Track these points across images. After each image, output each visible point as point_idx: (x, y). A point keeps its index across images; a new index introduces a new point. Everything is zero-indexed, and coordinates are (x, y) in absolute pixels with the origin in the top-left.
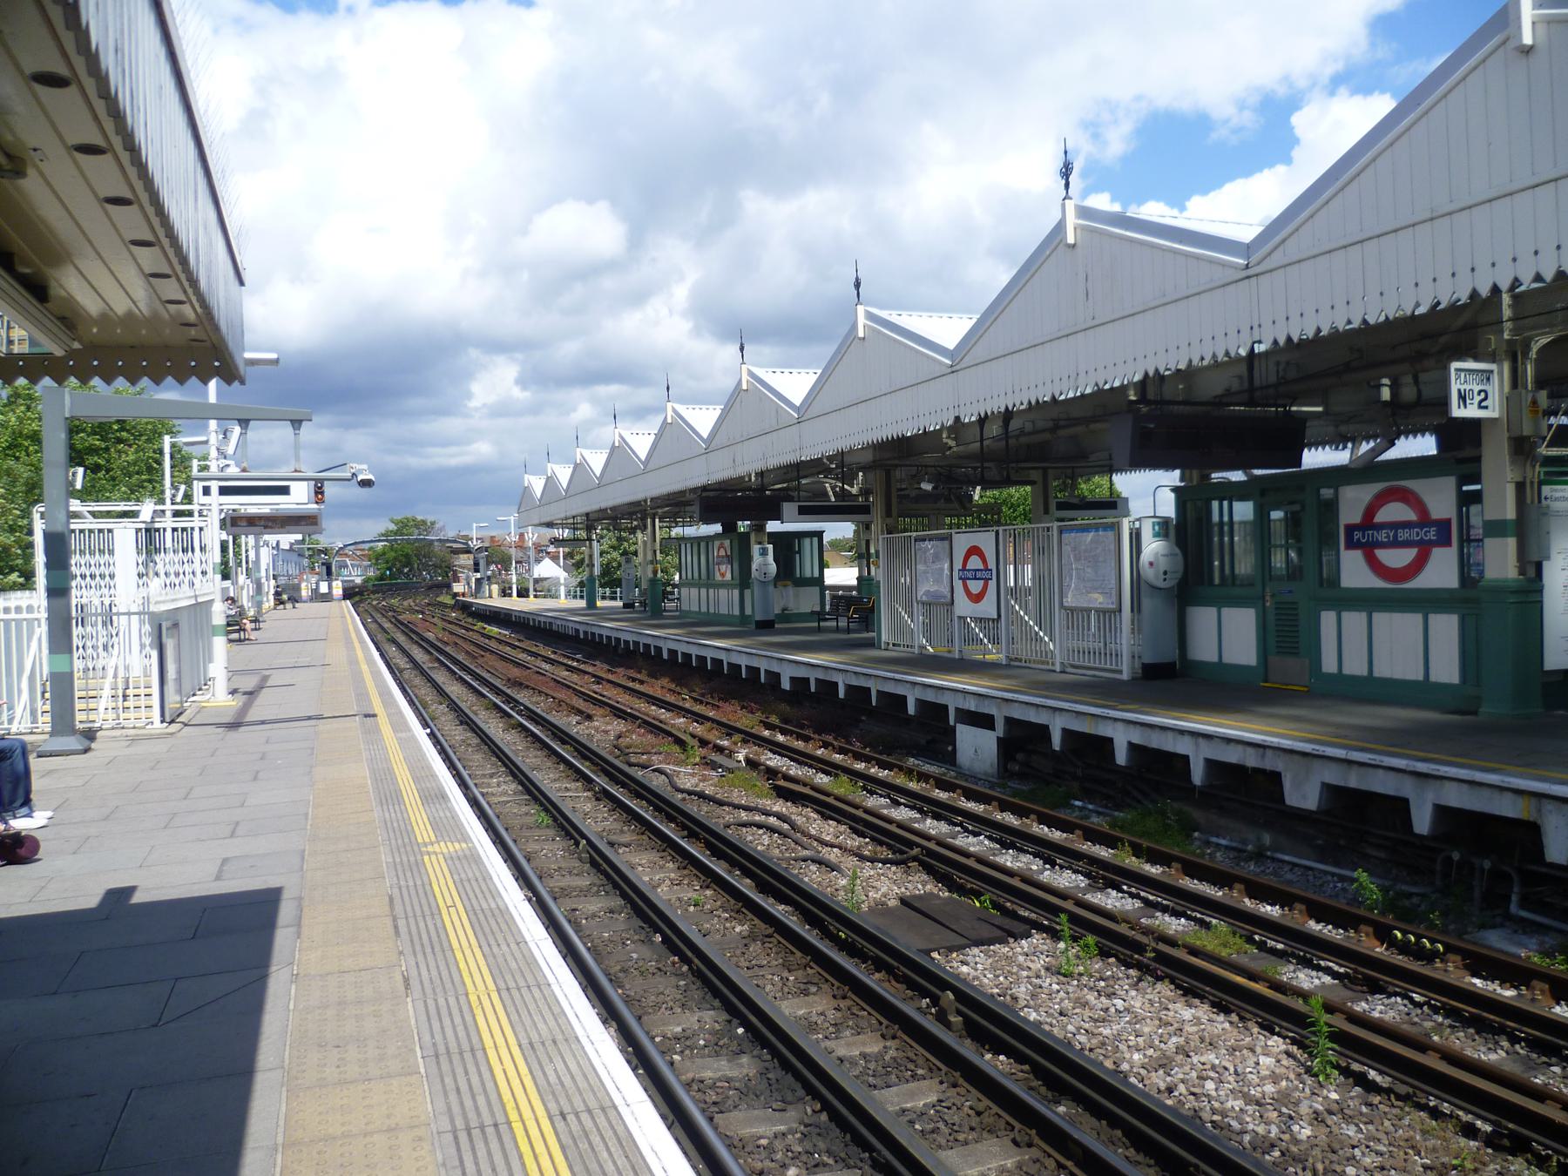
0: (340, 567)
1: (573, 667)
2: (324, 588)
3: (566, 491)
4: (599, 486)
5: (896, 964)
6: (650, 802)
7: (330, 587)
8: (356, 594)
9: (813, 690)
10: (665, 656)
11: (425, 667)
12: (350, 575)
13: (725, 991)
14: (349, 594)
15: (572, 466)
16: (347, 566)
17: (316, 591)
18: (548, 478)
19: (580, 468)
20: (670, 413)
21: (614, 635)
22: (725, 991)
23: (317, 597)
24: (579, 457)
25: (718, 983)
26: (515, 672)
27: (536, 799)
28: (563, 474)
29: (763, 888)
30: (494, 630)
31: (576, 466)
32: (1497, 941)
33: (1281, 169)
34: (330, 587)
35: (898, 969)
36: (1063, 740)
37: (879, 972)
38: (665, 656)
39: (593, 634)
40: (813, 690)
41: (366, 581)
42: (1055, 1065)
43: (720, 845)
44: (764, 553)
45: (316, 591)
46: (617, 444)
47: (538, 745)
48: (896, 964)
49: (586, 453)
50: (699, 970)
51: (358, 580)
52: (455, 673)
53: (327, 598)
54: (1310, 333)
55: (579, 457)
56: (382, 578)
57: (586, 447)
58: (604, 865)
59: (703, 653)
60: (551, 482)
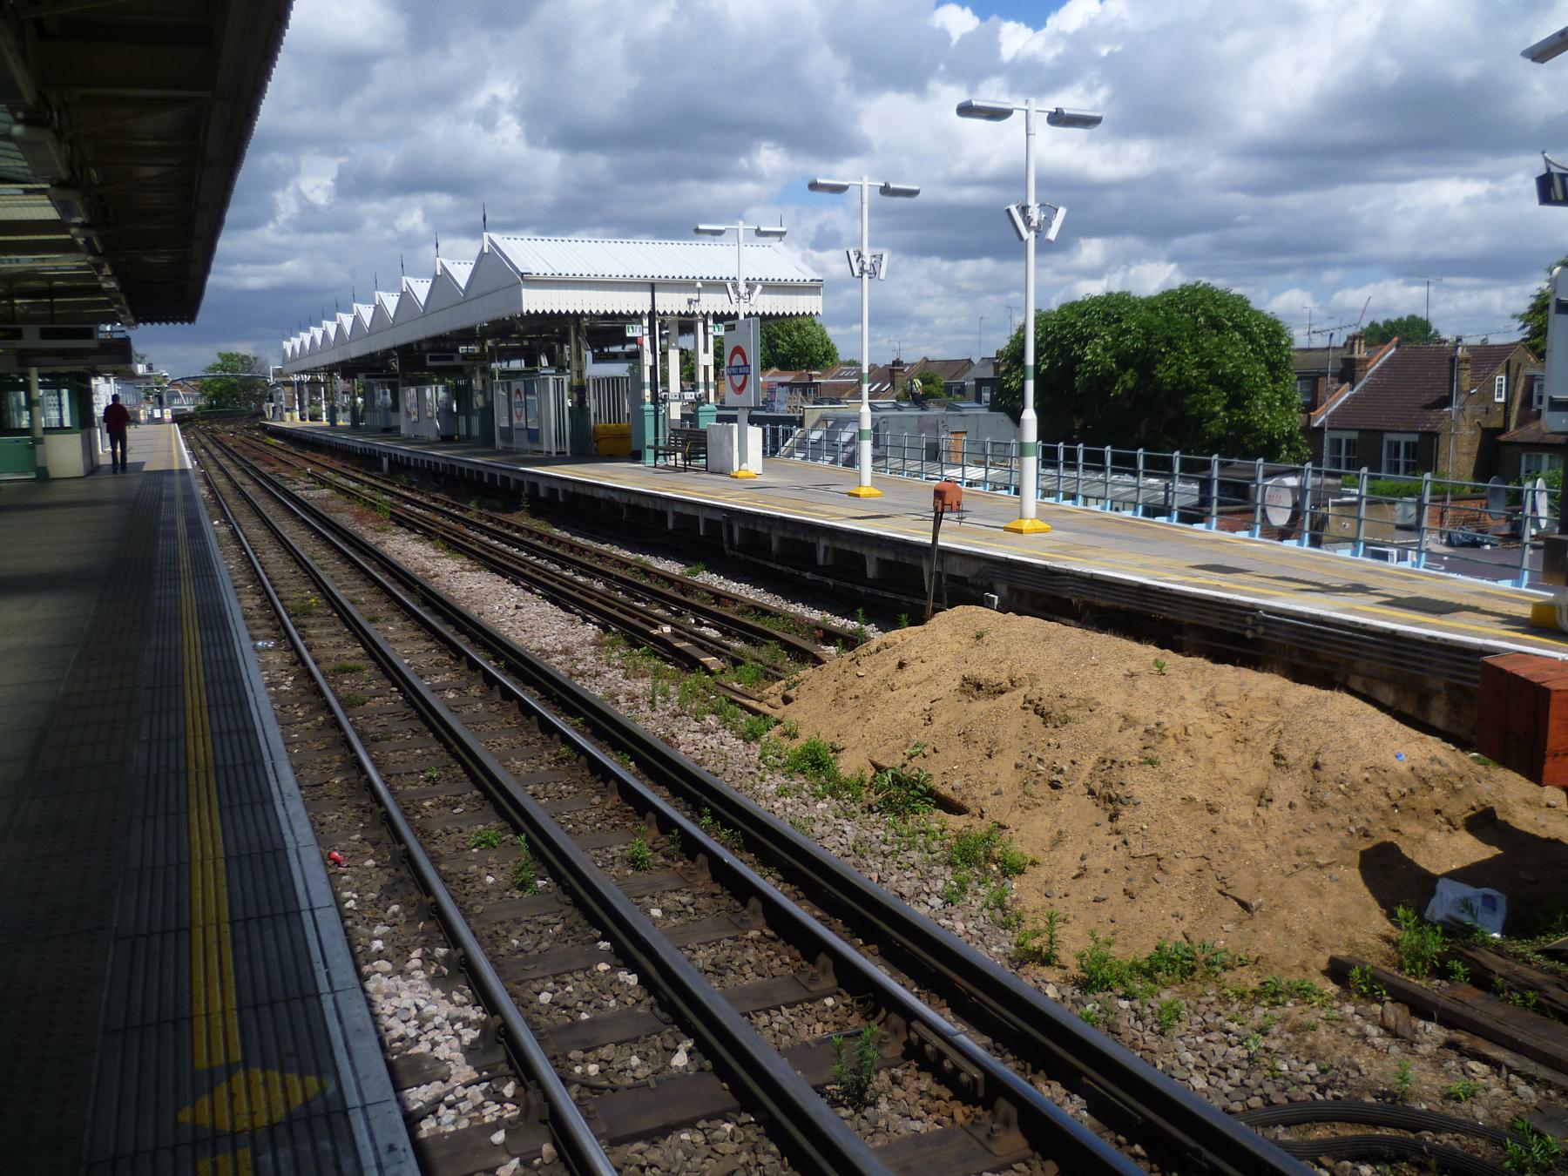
0: (173, 397)
1: (516, 539)
2: (157, 414)
3: (425, 308)
4: (369, 335)
5: (1192, 1144)
6: (635, 757)
7: (162, 413)
8: (186, 420)
9: (670, 526)
10: (486, 480)
11: (423, 686)
12: (182, 404)
13: (721, 1049)
14: (179, 418)
15: (431, 281)
16: (179, 396)
17: (151, 416)
18: (402, 293)
19: (406, 298)
20: (486, 243)
21: (413, 457)
22: (721, 1049)
23: (152, 420)
24: (404, 285)
25: (491, 787)
26: (255, 453)
27: (319, 589)
28: (391, 302)
29: (511, 670)
30: (273, 441)
31: (436, 278)
32: (438, 495)
33: (1030, 31)
34: (162, 413)
35: (1198, 1153)
36: (675, 523)
37: (749, 851)
38: (486, 480)
39: (422, 461)
40: (670, 526)
41: (199, 408)
42: (1042, 1033)
43: (671, 774)
44: (385, 393)
45: (151, 416)
46: (486, 250)
47: (385, 596)
48: (1192, 1144)
49: (411, 281)
50: (410, 698)
51: (190, 409)
52: (297, 515)
53: (160, 421)
54: (602, 312)
55: (404, 285)
56: (211, 406)
57: (413, 276)
58: (456, 747)
59: (430, 459)
60: (357, 321)
